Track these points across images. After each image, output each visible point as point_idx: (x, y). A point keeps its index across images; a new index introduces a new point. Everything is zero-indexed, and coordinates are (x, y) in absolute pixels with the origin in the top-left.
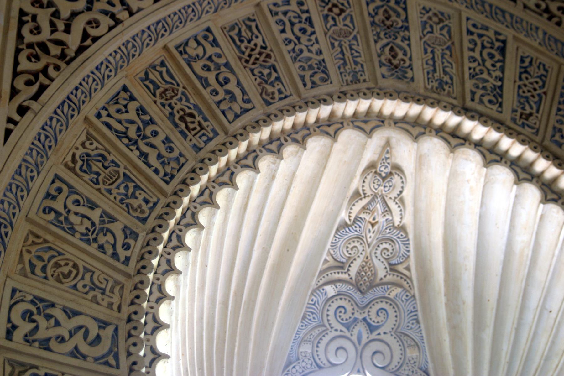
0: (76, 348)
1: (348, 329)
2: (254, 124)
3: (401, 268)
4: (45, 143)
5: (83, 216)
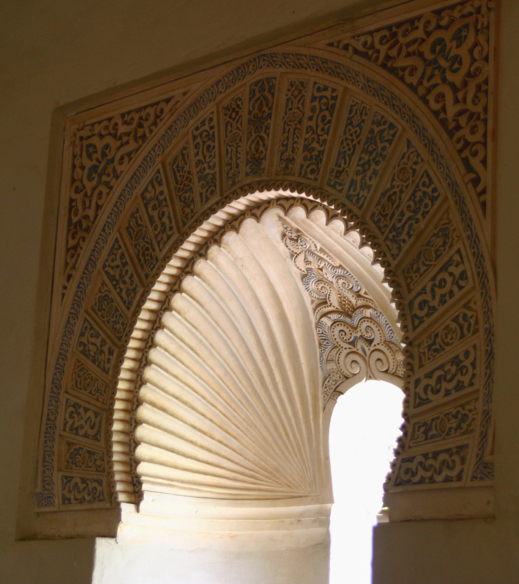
1: (354, 346)
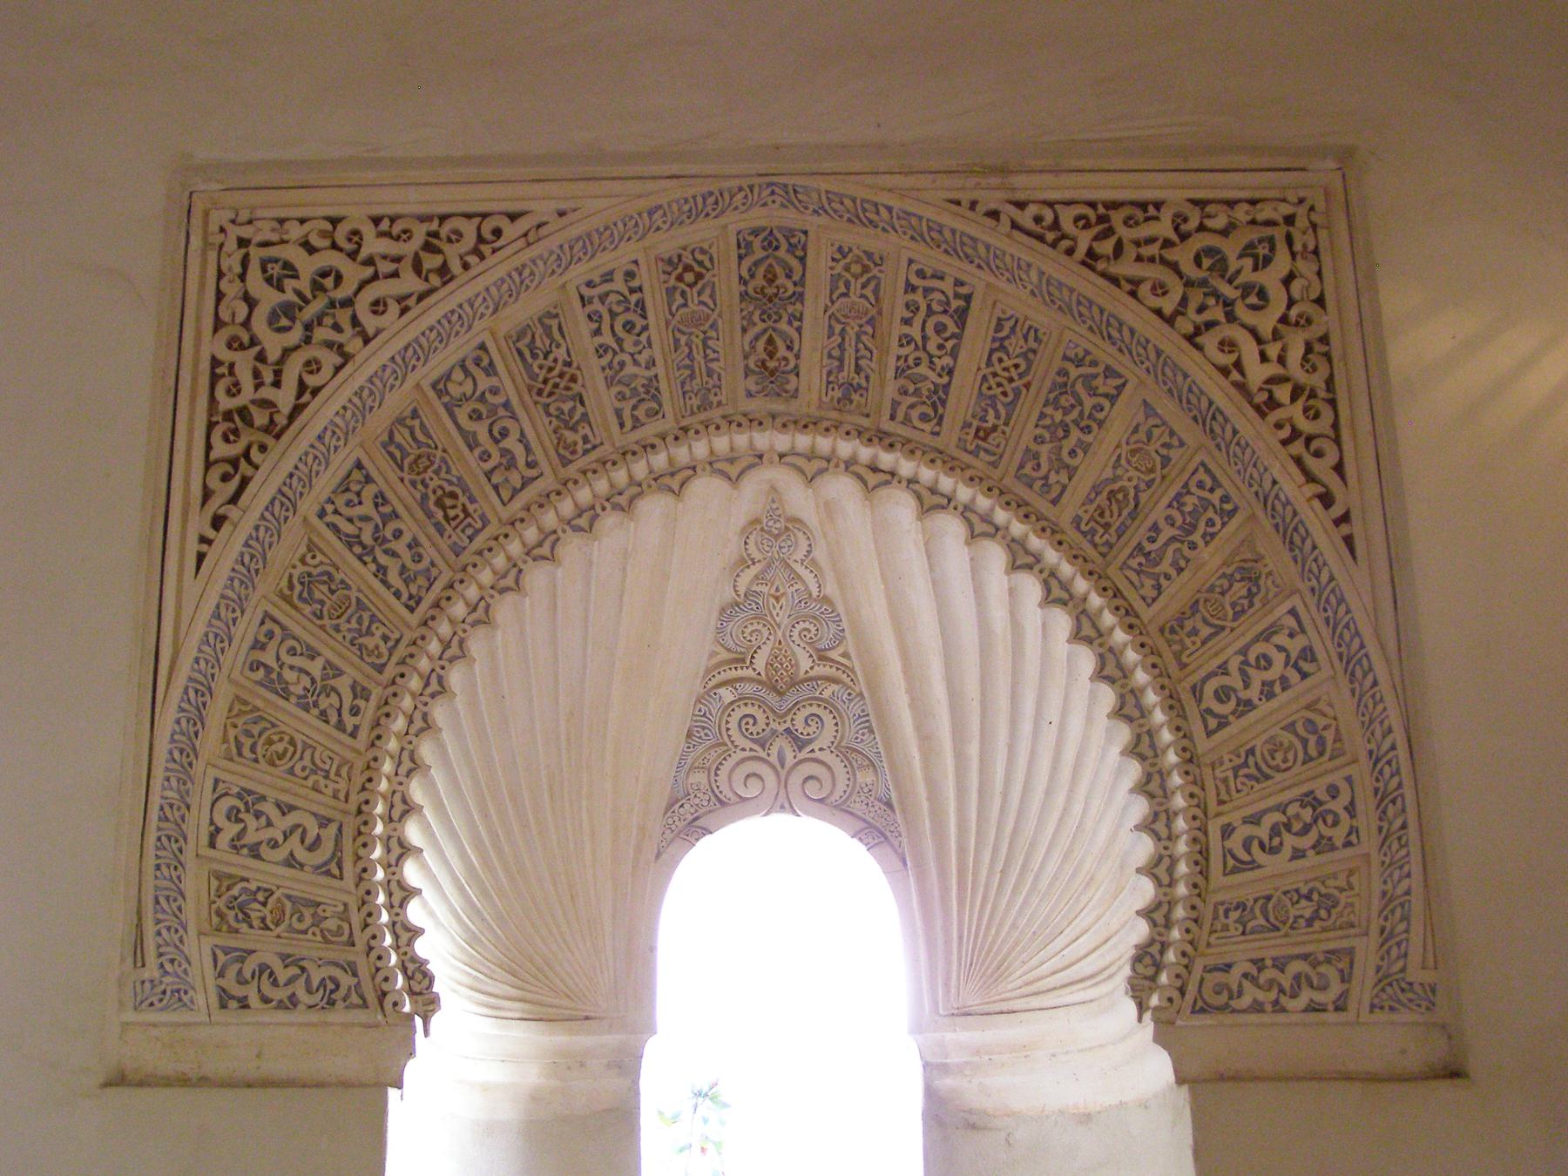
0: (291, 854)
1: (763, 746)
2: (543, 500)
3: (834, 655)
4: (249, 569)
5: (301, 670)
